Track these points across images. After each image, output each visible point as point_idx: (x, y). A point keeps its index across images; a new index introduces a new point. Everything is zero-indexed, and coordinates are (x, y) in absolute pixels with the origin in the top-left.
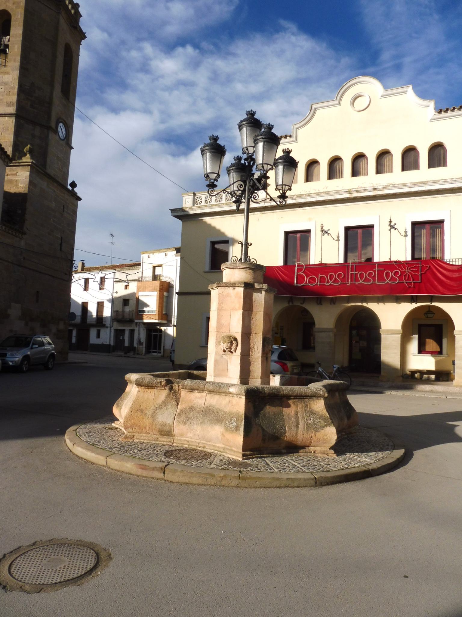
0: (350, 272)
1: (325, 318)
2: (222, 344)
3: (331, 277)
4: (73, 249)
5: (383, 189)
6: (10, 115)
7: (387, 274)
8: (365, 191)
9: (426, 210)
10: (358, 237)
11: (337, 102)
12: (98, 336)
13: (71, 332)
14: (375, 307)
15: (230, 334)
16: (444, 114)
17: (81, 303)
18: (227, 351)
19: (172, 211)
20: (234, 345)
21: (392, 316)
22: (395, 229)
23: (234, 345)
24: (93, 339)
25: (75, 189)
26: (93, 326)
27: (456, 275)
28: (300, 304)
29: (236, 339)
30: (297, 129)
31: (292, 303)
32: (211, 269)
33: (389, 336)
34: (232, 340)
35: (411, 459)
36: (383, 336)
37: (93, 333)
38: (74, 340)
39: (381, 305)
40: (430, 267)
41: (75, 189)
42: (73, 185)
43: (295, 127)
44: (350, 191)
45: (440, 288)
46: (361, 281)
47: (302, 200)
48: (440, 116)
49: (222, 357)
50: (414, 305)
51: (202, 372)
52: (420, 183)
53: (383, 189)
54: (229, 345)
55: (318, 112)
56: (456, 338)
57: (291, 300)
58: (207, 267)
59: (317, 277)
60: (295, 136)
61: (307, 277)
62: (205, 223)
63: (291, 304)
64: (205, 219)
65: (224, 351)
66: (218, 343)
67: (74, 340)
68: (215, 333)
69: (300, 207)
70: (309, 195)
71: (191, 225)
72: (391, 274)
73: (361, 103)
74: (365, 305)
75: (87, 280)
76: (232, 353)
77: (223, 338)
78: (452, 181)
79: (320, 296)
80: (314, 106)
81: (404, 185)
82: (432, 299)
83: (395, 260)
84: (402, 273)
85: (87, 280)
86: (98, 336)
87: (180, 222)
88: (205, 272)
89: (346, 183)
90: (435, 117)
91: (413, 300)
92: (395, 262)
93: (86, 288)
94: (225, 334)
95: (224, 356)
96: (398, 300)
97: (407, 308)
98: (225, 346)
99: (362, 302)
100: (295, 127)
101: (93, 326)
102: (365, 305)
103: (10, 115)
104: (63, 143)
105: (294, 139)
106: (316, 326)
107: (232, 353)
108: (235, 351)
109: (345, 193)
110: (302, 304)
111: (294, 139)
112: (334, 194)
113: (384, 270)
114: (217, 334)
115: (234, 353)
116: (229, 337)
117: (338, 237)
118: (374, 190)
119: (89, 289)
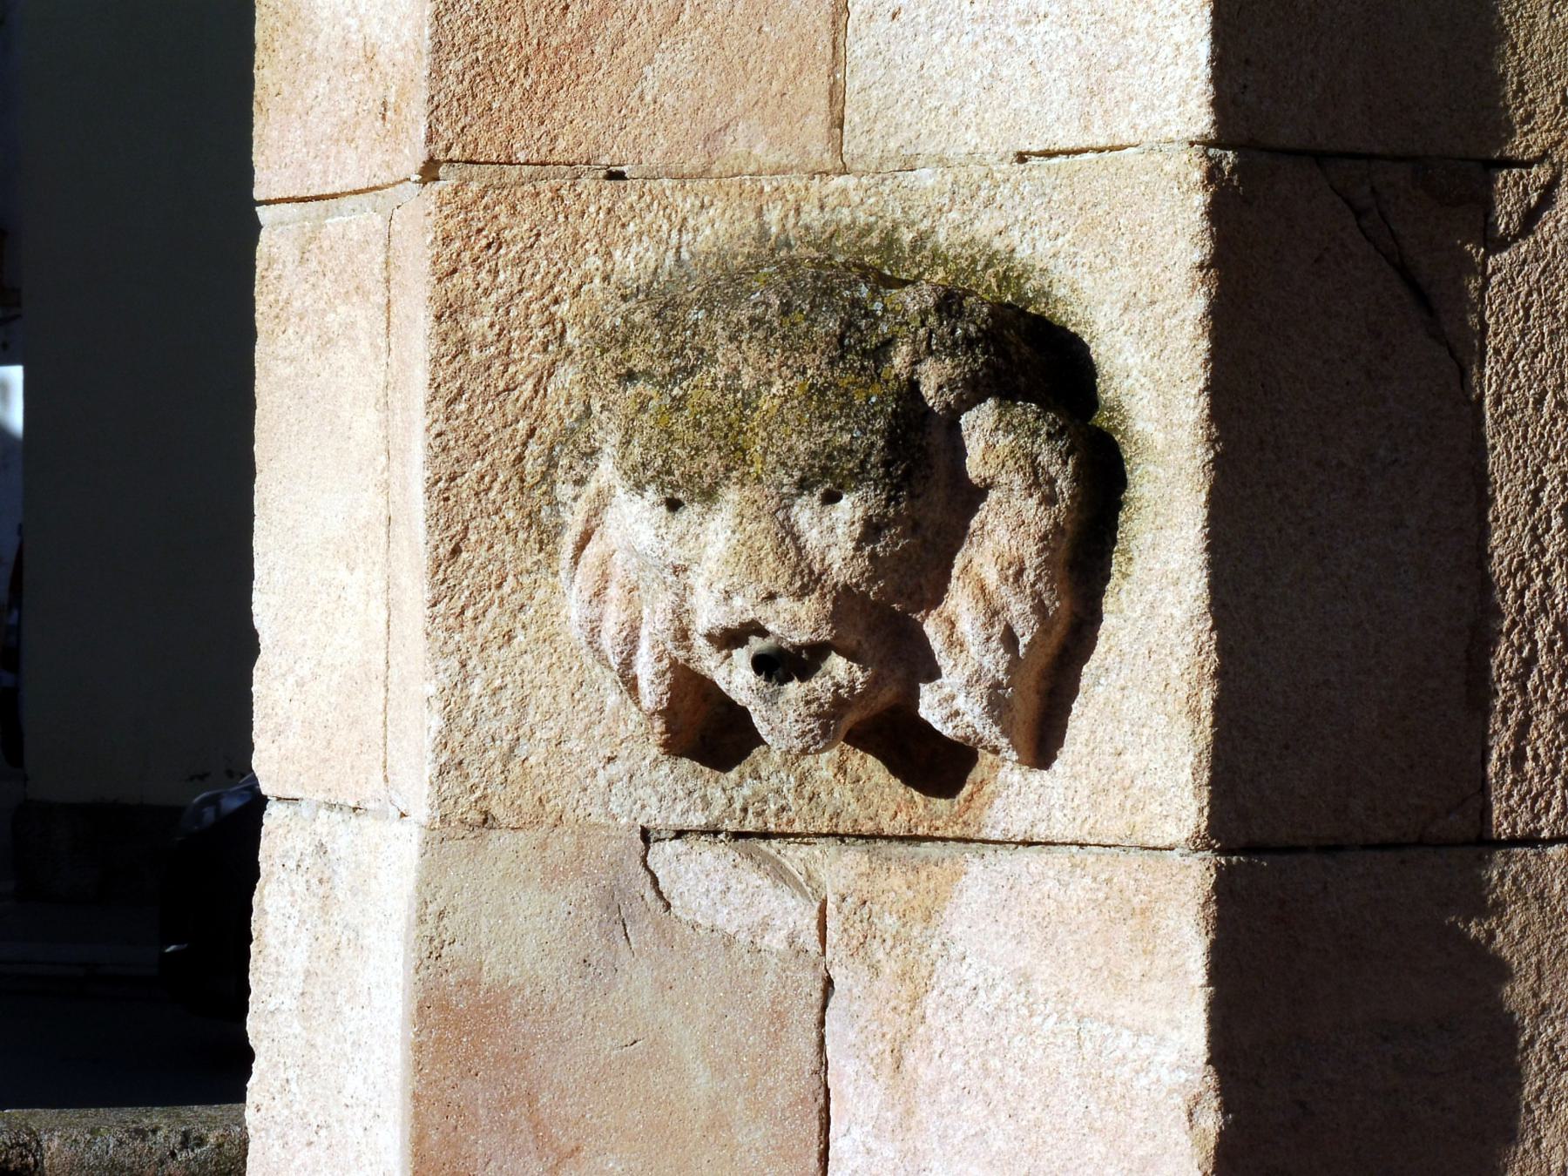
2: (634, 521)
6: (261, 203)
15: (848, 204)
18: (781, 715)
20: (1003, 540)
23: (1003, 540)
29: (1039, 361)
31: (973, 391)
34: (926, 387)
49: (628, 901)
51: (197, 1116)
54: (834, 531)
65: (707, 730)
66: (494, 502)
68: (417, 216)
76: (937, 765)
77: (663, 326)
94: (715, 228)
95: (701, 880)
98: (686, 566)
103: (261, 203)
107: (937, 765)
108: (1041, 713)
114: (465, 251)
115: (1010, 793)
116: (837, 294)
119: (1056, 765)
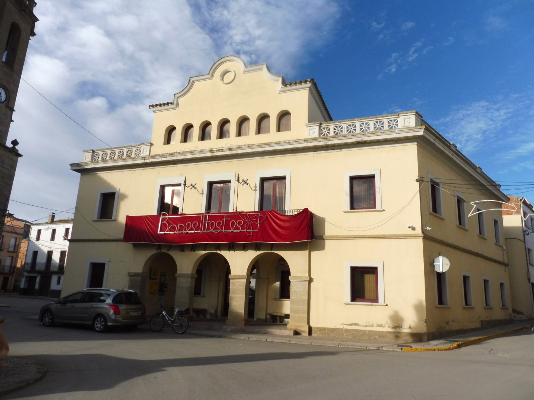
0: (204, 222)
1: (186, 263)
3: (189, 225)
4: (8, 200)
5: (237, 149)
7: (233, 224)
8: (223, 150)
9: (272, 167)
10: (216, 191)
11: (209, 76)
12: (59, 283)
13: (35, 278)
14: (226, 254)
16: (289, 87)
17: (46, 252)
19: (72, 165)
21: (239, 262)
22: (247, 184)
24: (54, 286)
25: (17, 147)
26: (55, 273)
27: (287, 224)
28: (166, 251)
30: (178, 98)
32: (100, 218)
33: (236, 280)
35: (90, 389)
36: (231, 281)
37: (54, 279)
38: (37, 286)
39: (231, 252)
40: (267, 217)
41: (17, 147)
42: (15, 143)
43: (176, 96)
44: (211, 151)
45: (273, 236)
46: (211, 231)
47: (174, 158)
48: (286, 89)
50: (258, 253)
52: (265, 144)
53: (237, 149)
55: (196, 84)
56: (291, 283)
57: (159, 247)
58: (95, 217)
59: (177, 225)
60: (175, 103)
61: (169, 225)
62: (99, 177)
63: (159, 251)
64: (101, 174)
67: (37, 286)
69: (174, 164)
70: (179, 153)
71: (88, 178)
72: (236, 224)
73: (228, 77)
74: (218, 252)
75: (54, 231)
78: (289, 143)
79: (186, 244)
80: (192, 79)
81: (253, 145)
82: (272, 247)
83: (240, 211)
84: (245, 222)
85: (54, 231)
86: (59, 283)
87: (79, 174)
88: (94, 221)
89: (214, 143)
90: (283, 89)
91: (257, 247)
92: (240, 212)
93: (53, 239)
96: (245, 248)
97: (251, 255)
99: (216, 250)
100: (176, 96)
101: (55, 273)
102: (218, 252)
104: (3, 106)
105: (174, 106)
106: (178, 272)
109: (207, 152)
110: (168, 251)
111: (174, 106)
112: (199, 153)
113: (231, 220)
117: (203, 191)
118: (230, 149)
